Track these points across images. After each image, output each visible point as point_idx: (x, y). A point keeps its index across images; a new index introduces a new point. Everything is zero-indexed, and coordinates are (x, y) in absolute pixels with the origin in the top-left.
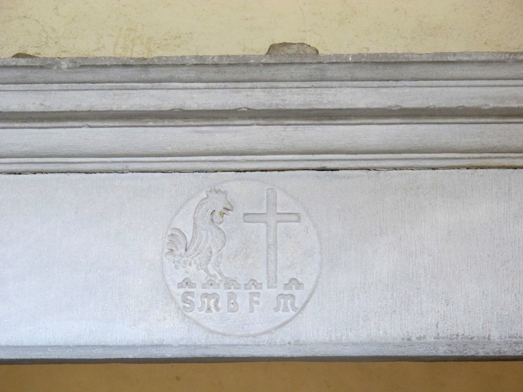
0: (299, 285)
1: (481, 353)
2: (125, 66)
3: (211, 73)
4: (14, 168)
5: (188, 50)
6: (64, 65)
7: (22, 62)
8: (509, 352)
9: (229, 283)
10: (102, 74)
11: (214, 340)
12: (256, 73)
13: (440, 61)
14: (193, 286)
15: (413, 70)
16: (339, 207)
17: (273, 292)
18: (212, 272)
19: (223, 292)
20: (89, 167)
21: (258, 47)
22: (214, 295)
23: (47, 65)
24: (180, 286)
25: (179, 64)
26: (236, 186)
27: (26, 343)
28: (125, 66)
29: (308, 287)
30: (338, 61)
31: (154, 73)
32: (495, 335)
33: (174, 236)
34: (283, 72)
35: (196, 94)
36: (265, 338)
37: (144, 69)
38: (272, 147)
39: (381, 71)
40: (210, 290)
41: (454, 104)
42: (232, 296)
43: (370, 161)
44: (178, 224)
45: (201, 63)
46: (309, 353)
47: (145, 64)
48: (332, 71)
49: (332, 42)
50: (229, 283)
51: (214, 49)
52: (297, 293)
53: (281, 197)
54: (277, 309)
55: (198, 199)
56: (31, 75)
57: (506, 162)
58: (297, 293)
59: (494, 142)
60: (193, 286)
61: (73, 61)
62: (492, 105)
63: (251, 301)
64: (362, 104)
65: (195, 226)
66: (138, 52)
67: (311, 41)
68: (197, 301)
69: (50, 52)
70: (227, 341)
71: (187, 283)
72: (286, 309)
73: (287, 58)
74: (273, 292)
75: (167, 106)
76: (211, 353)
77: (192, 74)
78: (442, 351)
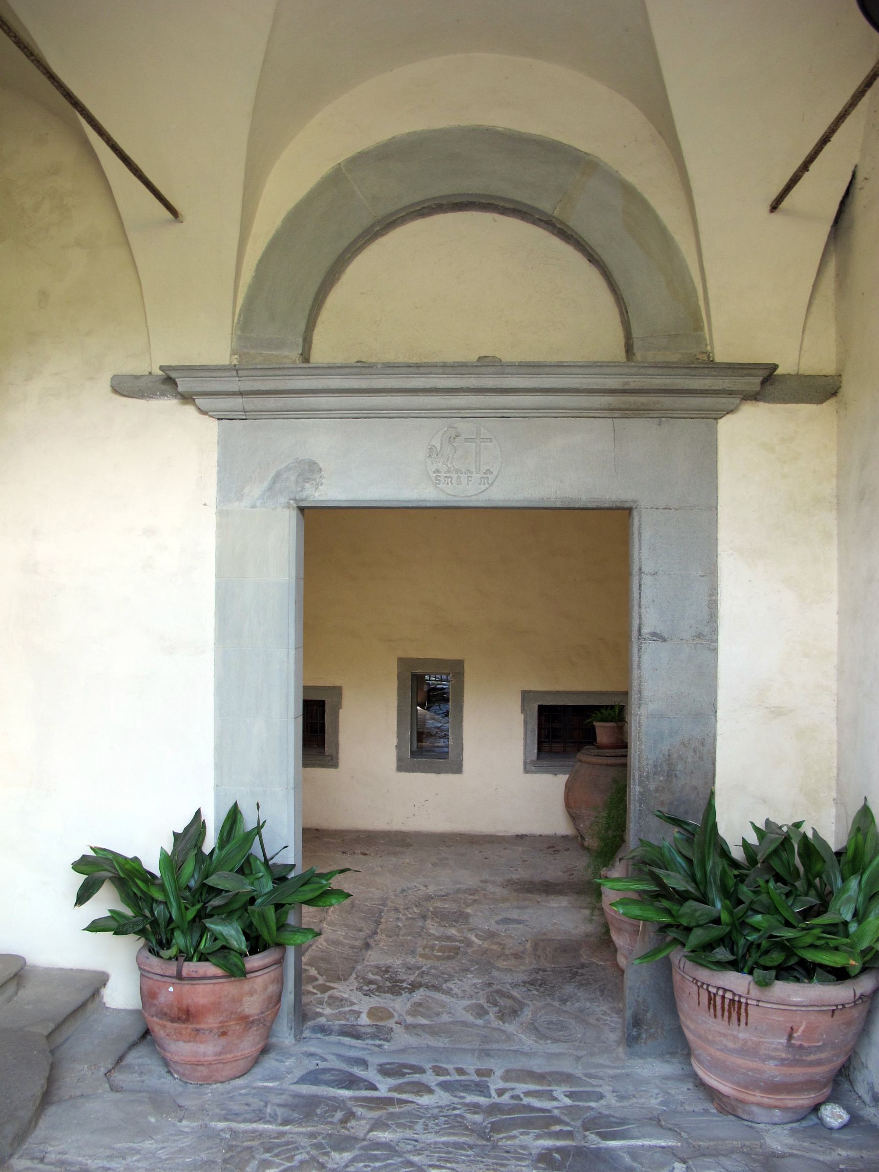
0: (491, 473)
1: (577, 506)
2: (409, 366)
3: (449, 370)
4: (356, 416)
5: (439, 359)
6: (379, 366)
7: (359, 364)
8: (590, 505)
9: (457, 471)
10: (397, 370)
11: (450, 498)
12: (472, 370)
13: (560, 365)
14: (440, 472)
15: (547, 370)
16: (652, 788)
17: (479, 476)
18: (450, 466)
19: (454, 476)
20: (391, 415)
21: (473, 357)
22: (450, 477)
23: (371, 366)
24: (434, 472)
25: (434, 366)
26: (463, 426)
27: (361, 499)
28: (409, 366)
29: (495, 473)
30: (511, 365)
31: (422, 370)
32: (584, 498)
33: (432, 449)
34: (483, 370)
35: (724, 400)
36: (475, 497)
37: (418, 368)
38: (478, 406)
39: (531, 370)
40: (448, 475)
41: (566, 386)
42: (459, 477)
43: (526, 413)
44: (433, 443)
45: (445, 366)
46: (495, 505)
47: (418, 366)
48: (508, 370)
49: (509, 356)
50: (457, 471)
51: (452, 357)
52: (490, 476)
53: (483, 430)
54: (480, 484)
55: (443, 432)
56: (364, 371)
57: (591, 415)
58: (490, 476)
59: (585, 405)
60: (440, 472)
61: (383, 364)
62: (584, 387)
63: (468, 481)
64: (522, 386)
65: (441, 444)
66: (415, 360)
67: (498, 355)
68: (442, 479)
69: (373, 360)
70: (456, 499)
71: (437, 471)
72: (484, 484)
73: (486, 364)
74: (479, 476)
75: (429, 386)
76: (449, 504)
77: (440, 370)
78: (558, 505)
